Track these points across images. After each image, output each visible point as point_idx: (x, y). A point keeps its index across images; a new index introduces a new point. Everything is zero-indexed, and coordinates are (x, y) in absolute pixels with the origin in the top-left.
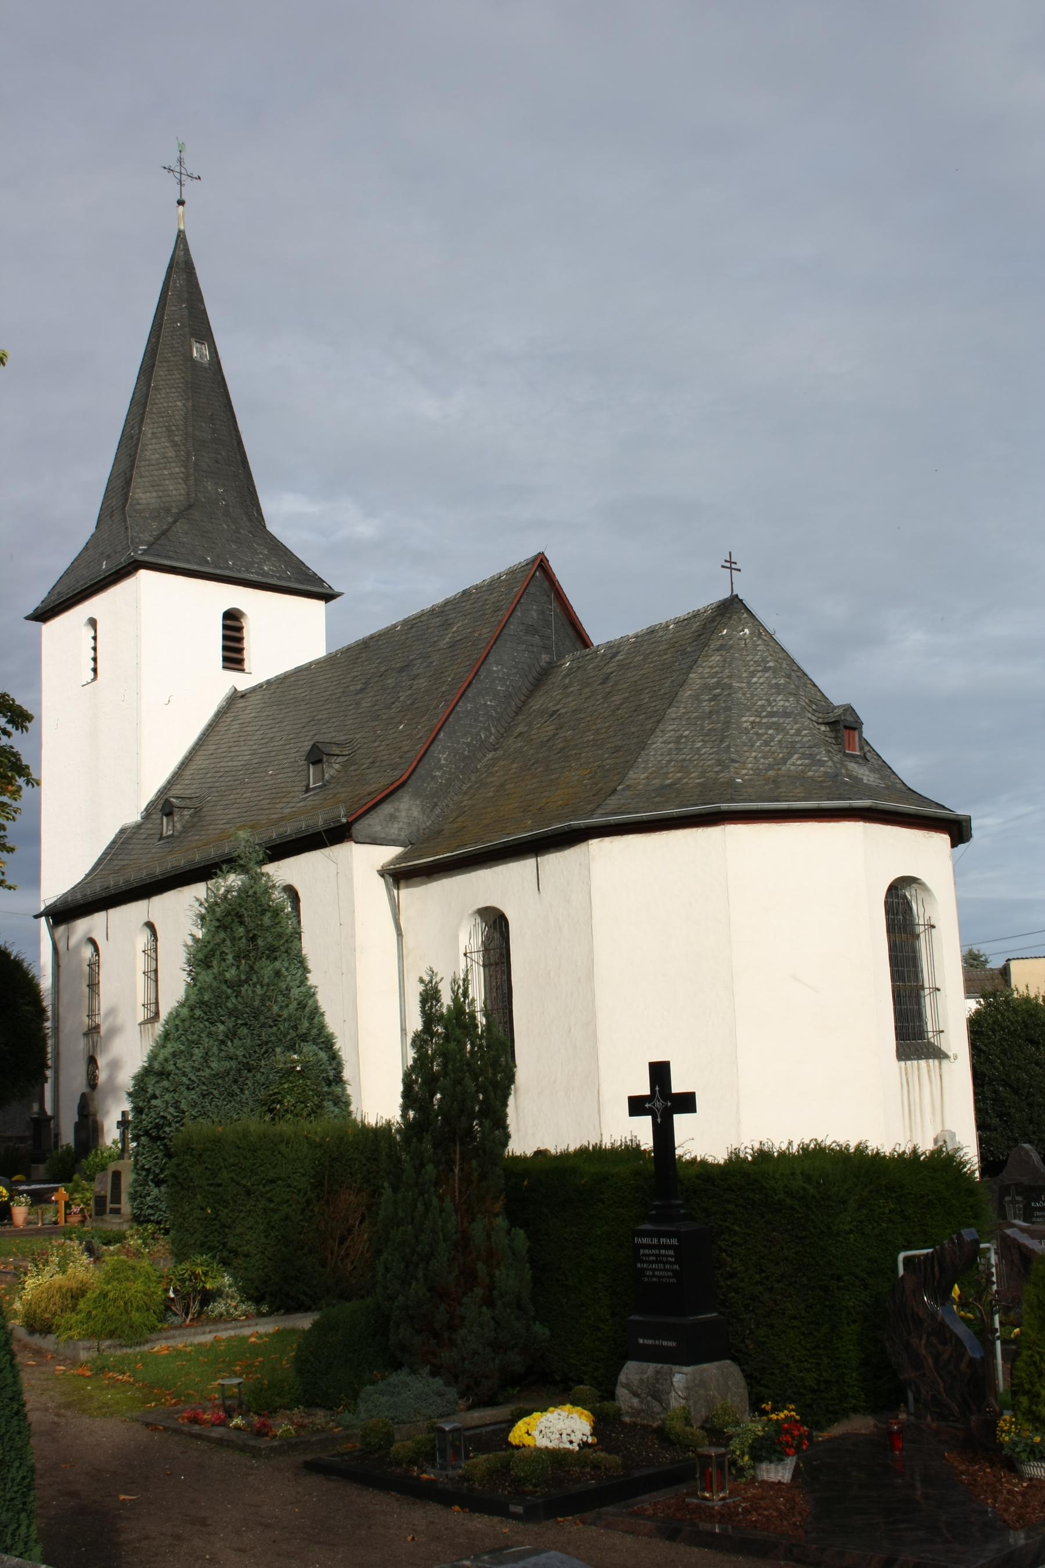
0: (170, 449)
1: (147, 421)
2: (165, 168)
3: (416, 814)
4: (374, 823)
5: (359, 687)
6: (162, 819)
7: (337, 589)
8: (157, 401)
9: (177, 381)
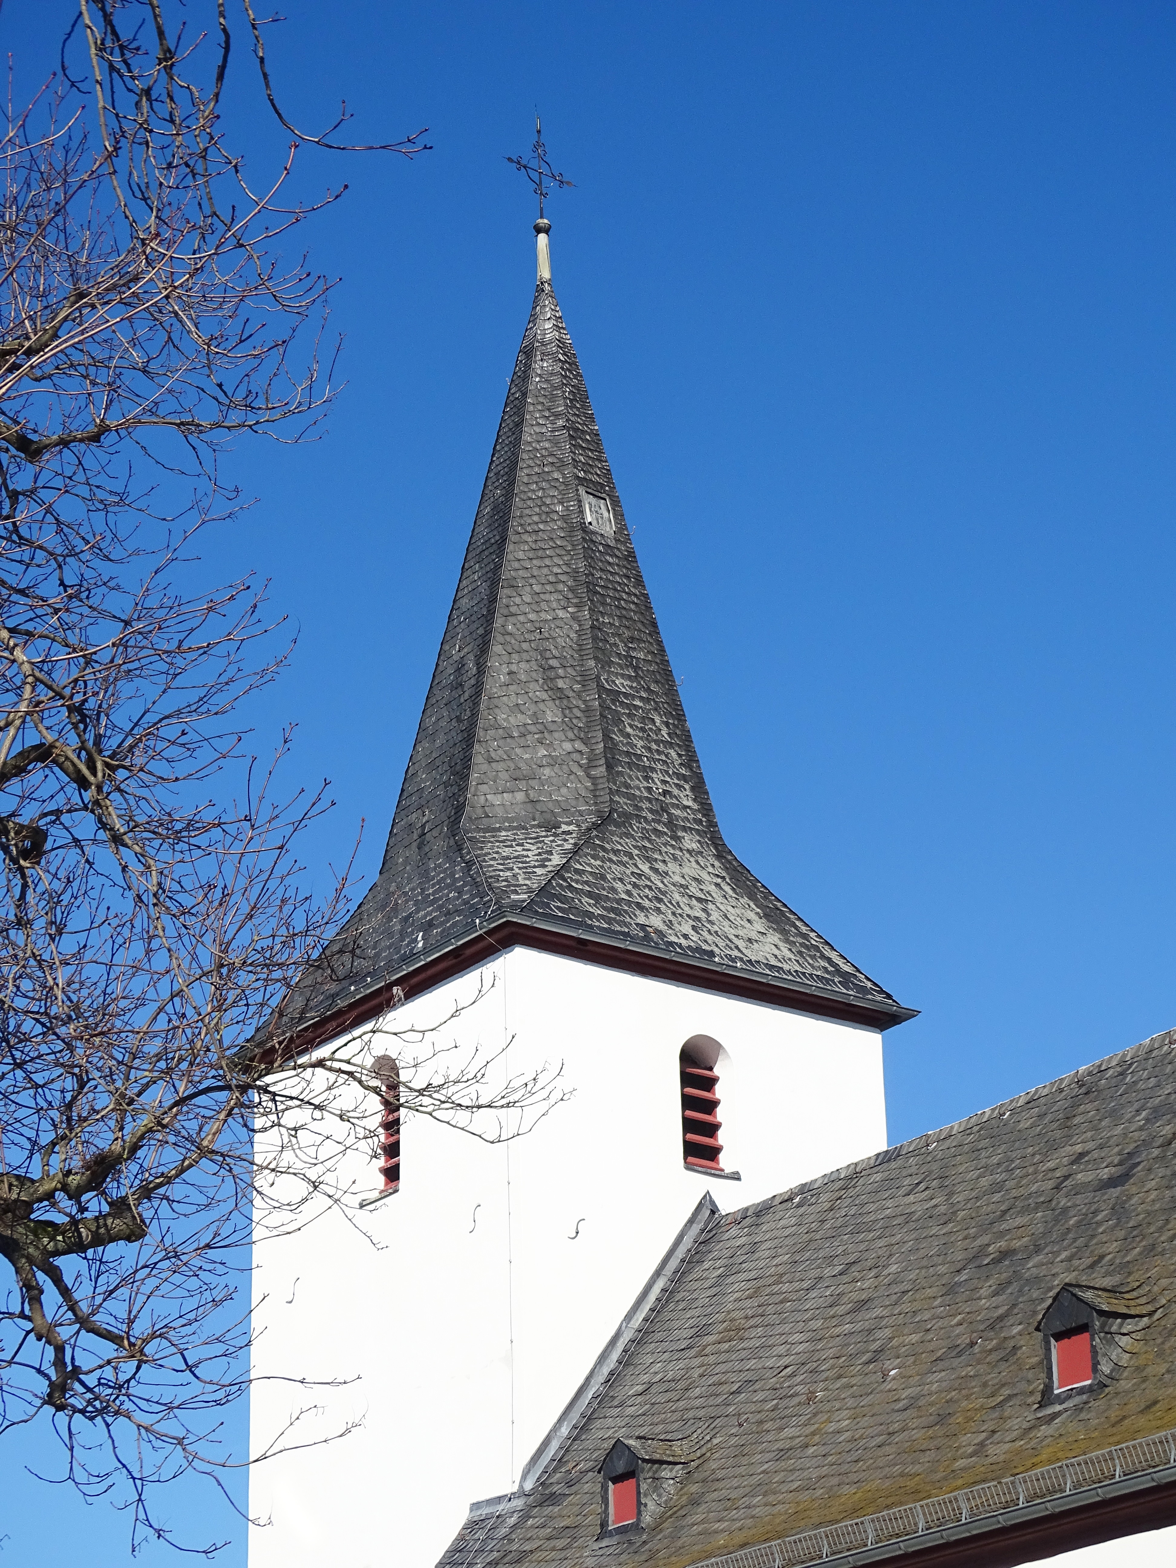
0: (550, 704)
1: (497, 649)
2: (509, 159)
5: (1105, 1173)
6: (605, 1488)
7: (905, 1002)
8: (513, 609)
9: (556, 570)
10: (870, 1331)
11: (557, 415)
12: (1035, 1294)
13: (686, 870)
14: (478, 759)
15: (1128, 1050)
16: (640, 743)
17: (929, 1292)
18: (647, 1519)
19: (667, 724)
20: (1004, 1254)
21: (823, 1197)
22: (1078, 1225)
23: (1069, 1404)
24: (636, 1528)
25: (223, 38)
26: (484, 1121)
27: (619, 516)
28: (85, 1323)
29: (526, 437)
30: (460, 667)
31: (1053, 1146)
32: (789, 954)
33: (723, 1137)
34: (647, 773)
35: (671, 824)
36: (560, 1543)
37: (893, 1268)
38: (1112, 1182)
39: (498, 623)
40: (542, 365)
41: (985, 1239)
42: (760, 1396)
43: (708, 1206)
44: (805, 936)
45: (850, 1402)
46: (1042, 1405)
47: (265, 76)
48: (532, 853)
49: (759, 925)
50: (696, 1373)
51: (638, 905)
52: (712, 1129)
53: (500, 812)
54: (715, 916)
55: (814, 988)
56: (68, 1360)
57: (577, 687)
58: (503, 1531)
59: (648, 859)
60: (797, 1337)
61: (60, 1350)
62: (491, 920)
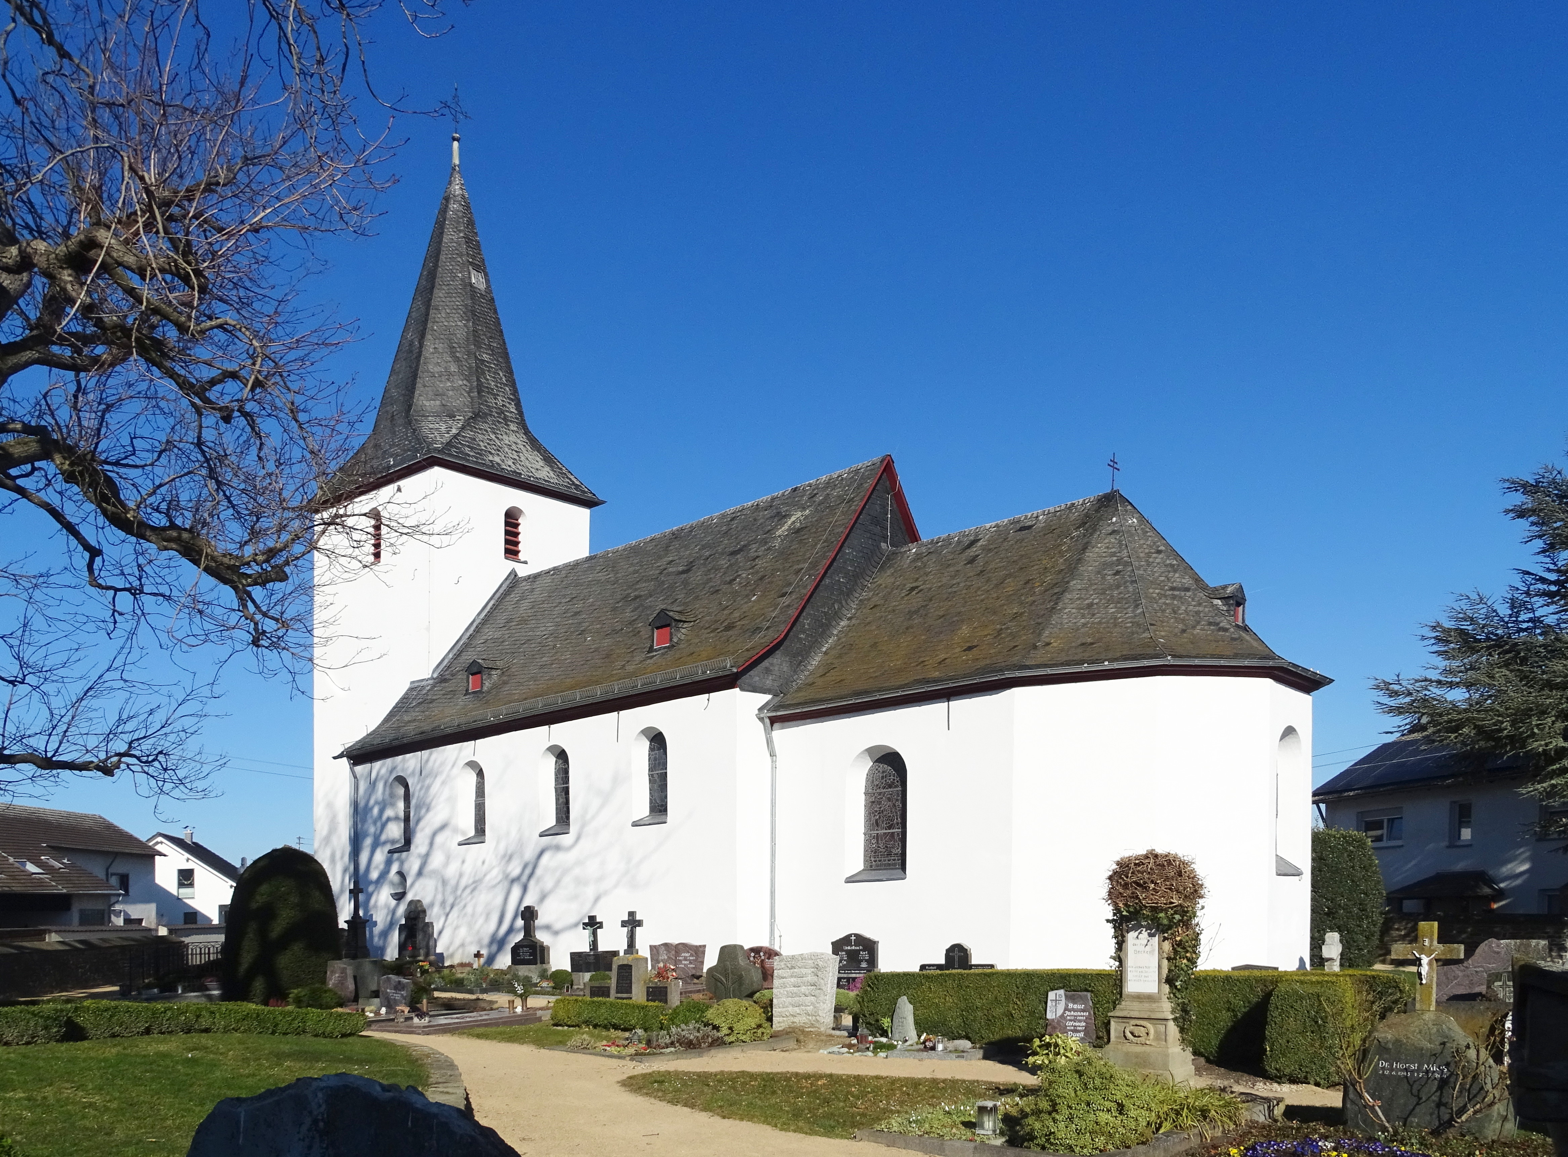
1: (429, 337)
3: (785, 669)
4: (755, 675)
5: (681, 569)
6: (468, 678)
7: (601, 498)
8: (437, 320)
10: (580, 623)
11: (460, 231)
12: (649, 612)
13: (511, 439)
14: (419, 385)
15: (694, 522)
16: (493, 383)
17: (605, 610)
18: (485, 689)
19: (505, 376)
20: (636, 597)
21: (563, 572)
22: (668, 587)
23: (660, 652)
24: (481, 692)
25: (345, 50)
26: (435, 540)
27: (487, 281)
28: (265, 615)
29: (445, 240)
30: (411, 344)
31: (660, 557)
32: (553, 476)
33: (521, 547)
34: (495, 396)
35: (505, 419)
36: (449, 697)
37: (591, 600)
38: (683, 572)
39: (429, 325)
40: (454, 206)
41: (630, 591)
42: (533, 646)
43: (513, 573)
44: (561, 469)
45: (571, 649)
46: (649, 652)
47: (365, 70)
48: (443, 428)
49: (541, 463)
50: (507, 636)
51: (490, 452)
52: (517, 544)
53: (429, 409)
54: (523, 458)
55: (563, 490)
56: (260, 627)
57: (465, 357)
58: (424, 692)
59: (495, 433)
60: (549, 624)
61: (256, 624)
62: (425, 454)
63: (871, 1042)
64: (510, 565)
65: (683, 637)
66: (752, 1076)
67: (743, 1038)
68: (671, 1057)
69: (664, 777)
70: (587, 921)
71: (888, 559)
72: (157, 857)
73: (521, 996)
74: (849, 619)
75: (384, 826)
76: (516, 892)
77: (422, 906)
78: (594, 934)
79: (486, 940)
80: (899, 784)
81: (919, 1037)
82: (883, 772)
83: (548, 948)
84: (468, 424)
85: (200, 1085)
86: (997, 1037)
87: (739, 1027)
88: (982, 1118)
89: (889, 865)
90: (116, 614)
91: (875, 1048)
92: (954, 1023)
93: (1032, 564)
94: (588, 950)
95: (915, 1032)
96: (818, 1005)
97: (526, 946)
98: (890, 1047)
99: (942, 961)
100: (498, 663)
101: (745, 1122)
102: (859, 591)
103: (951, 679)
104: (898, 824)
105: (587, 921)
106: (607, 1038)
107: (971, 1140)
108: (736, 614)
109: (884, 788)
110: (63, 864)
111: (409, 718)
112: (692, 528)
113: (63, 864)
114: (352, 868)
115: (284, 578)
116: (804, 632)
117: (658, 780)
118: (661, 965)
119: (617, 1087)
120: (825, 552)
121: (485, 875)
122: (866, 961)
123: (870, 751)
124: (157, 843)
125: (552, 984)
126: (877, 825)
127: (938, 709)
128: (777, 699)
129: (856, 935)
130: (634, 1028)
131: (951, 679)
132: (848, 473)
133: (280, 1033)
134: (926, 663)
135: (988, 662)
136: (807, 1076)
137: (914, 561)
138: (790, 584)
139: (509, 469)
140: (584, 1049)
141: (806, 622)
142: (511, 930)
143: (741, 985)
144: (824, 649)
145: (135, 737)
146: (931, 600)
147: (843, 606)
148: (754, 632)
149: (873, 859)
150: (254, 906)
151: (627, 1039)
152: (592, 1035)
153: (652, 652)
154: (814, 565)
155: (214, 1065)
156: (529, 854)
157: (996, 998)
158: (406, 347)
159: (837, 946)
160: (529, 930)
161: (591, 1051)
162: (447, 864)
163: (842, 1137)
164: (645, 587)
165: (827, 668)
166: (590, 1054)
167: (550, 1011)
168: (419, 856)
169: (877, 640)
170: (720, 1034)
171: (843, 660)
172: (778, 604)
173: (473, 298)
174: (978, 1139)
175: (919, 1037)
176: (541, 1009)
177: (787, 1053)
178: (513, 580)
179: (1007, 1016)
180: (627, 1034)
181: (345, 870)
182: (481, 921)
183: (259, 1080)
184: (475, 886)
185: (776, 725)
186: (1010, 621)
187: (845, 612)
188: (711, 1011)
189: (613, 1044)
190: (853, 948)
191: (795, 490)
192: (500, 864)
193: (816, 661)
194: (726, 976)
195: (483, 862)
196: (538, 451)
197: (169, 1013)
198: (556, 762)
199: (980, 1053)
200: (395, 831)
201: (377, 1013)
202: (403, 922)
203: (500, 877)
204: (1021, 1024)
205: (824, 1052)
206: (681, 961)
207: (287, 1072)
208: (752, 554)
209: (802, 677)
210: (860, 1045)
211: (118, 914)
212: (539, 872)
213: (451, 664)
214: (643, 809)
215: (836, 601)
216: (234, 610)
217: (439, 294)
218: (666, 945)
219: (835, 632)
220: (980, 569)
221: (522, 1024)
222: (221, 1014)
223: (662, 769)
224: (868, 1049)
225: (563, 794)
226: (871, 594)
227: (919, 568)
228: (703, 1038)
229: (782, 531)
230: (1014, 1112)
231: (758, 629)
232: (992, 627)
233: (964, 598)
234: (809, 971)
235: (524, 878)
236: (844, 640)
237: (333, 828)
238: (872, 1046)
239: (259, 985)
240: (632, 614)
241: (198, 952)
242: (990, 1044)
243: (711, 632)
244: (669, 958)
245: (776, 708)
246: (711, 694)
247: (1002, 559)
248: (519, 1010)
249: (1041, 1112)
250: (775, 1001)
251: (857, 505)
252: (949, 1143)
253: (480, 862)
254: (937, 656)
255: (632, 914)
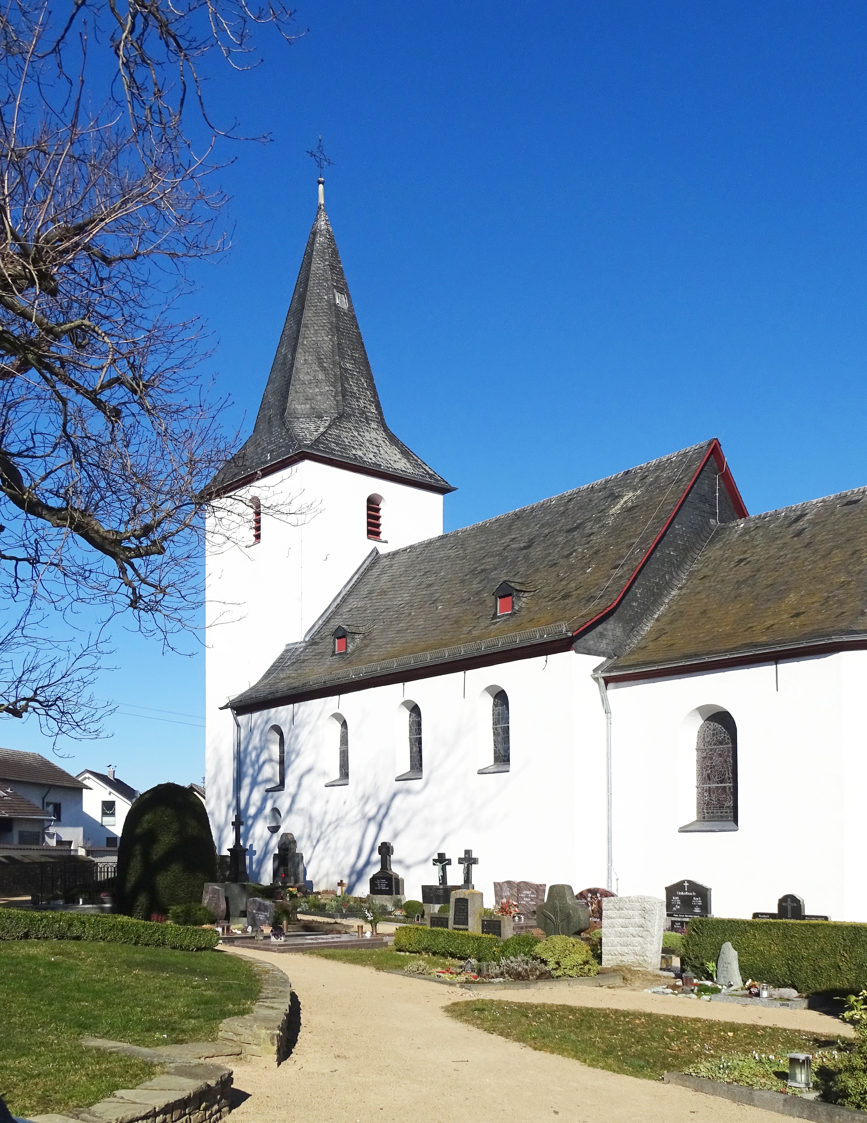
2: (308, 152)
4: (590, 639)
5: (522, 545)
6: (334, 641)
7: (453, 485)
10: (432, 594)
11: (326, 260)
12: (493, 584)
13: (372, 435)
14: (292, 392)
16: (355, 388)
18: (349, 650)
19: (366, 382)
20: (483, 571)
22: (511, 561)
24: (345, 653)
26: (292, 518)
27: (350, 301)
29: (313, 268)
31: (504, 535)
32: (410, 467)
33: (382, 529)
35: (366, 418)
36: (317, 657)
37: (442, 574)
38: (525, 548)
39: (300, 341)
40: (320, 239)
43: (375, 551)
44: (416, 461)
46: (492, 619)
47: (202, 104)
48: (312, 427)
49: (399, 456)
51: (354, 448)
53: (300, 412)
54: (382, 452)
55: (418, 478)
56: (137, 592)
57: (331, 366)
58: (298, 653)
59: (358, 431)
60: (406, 595)
61: (134, 589)
62: (296, 450)
63: (696, 985)
64: (372, 544)
65: (524, 605)
66: (571, 1010)
67: (570, 973)
68: (498, 987)
69: (507, 730)
70: (436, 857)
71: (717, 533)
72: (84, 790)
73: (371, 922)
74: (680, 589)
75: (260, 768)
76: (372, 829)
77: (293, 838)
78: (444, 870)
79: (347, 871)
80: (730, 741)
81: (745, 982)
82: (714, 730)
83: (403, 881)
84: (334, 424)
85: (54, 987)
86: (824, 988)
87: (566, 962)
88: (794, 1071)
89: (722, 817)
90: (18, 580)
91: (699, 991)
92: (780, 971)
93: (859, 535)
94: (438, 884)
95: (740, 978)
96: (645, 946)
97: (383, 878)
98: (715, 991)
99: (775, 910)
100: (361, 629)
101: (555, 1055)
102: (689, 563)
103: (778, 643)
104: (729, 778)
105: (436, 857)
106: (443, 966)
107: (781, 1092)
108: (573, 585)
109: (715, 744)
110: (6, 793)
111: (284, 676)
112: (533, 509)
113: (6, 793)
114: (234, 803)
115: (161, 551)
116: (636, 601)
117: (501, 733)
118: (504, 900)
119: (441, 1013)
120: (655, 528)
121: (346, 814)
122: (699, 906)
123: (701, 710)
124: (85, 778)
125: (404, 913)
126: (709, 778)
127: (767, 670)
128: (611, 661)
129: (689, 882)
130: (470, 957)
131: (778, 643)
132: (677, 457)
133: (142, 944)
134: (754, 629)
135: (816, 627)
136: (626, 1014)
137: (742, 535)
138: (622, 557)
139: (370, 461)
140: (420, 974)
141: (638, 591)
142: (368, 863)
143: (569, 923)
144: (656, 616)
145: (40, 685)
146: (758, 570)
147: (673, 577)
148: (588, 601)
149: (705, 811)
150: (139, 830)
151: (461, 967)
152: (428, 962)
153: (496, 618)
154: (644, 540)
155: (70, 969)
156: (383, 797)
157: (822, 949)
158: (280, 361)
159: (671, 891)
160: (385, 862)
161: (426, 976)
162: (312, 803)
163: (650, 1078)
164: (490, 562)
165: (659, 633)
166: (424, 979)
167: (394, 938)
168: (290, 794)
169: (705, 608)
170: (547, 968)
171: (673, 626)
172: (612, 575)
173: (337, 316)
174: (790, 1091)
175: (745, 982)
176: (389, 935)
177: (613, 990)
178: (375, 557)
179: (833, 967)
180: (462, 963)
181: (229, 806)
182: (342, 854)
183: (107, 986)
184: (337, 823)
185: (610, 685)
186: (837, 589)
187: (676, 583)
188: (539, 945)
189: (447, 971)
190: (687, 893)
191: (627, 473)
192: (359, 804)
193: (648, 627)
194: (555, 913)
195: (345, 803)
196: (397, 446)
197: (45, 921)
198: (410, 715)
199: (805, 1003)
200: (270, 771)
201: (244, 931)
202: (277, 852)
203: (359, 816)
204: (848, 977)
205: (648, 991)
206: (523, 898)
207: (134, 980)
208: (587, 531)
209: (635, 642)
210: (685, 987)
211: (51, 836)
212: (392, 812)
213: (321, 628)
214: (488, 759)
215: (667, 572)
216: (115, 577)
217: (308, 314)
218: (509, 883)
219: (667, 601)
220: (807, 541)
221: (371, 948)
222: (90, 924)
223: (505, 723)
224: (692, 991)
225: (417, 744)
226: (701, 565)
227: (747, 542)
228: (531, 970)
229: (616, 509)
230: (829, 1065)
231: (592, 598)
232: (819, 595)
233: (791, 569)
234: (636, 913)
235: (379, 817)
236: (674, 607)
237: (218, 770)
238: (696, 988)
239: (142, 900)
240: (478, 585)
241: (106, 870)
242: (817, 994)
243: (549, 601)
244: (512, 895)
245: (610, 669)
246: (548, 656)
247: (829, 531)
248: (368, 935)
249: (855, 1069)
250: (604, 940)
251: (686, 484)
252: (758, 1093)
253: (342, 803)
254: (765, 621)
255: (468, 852)
